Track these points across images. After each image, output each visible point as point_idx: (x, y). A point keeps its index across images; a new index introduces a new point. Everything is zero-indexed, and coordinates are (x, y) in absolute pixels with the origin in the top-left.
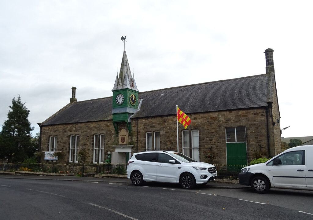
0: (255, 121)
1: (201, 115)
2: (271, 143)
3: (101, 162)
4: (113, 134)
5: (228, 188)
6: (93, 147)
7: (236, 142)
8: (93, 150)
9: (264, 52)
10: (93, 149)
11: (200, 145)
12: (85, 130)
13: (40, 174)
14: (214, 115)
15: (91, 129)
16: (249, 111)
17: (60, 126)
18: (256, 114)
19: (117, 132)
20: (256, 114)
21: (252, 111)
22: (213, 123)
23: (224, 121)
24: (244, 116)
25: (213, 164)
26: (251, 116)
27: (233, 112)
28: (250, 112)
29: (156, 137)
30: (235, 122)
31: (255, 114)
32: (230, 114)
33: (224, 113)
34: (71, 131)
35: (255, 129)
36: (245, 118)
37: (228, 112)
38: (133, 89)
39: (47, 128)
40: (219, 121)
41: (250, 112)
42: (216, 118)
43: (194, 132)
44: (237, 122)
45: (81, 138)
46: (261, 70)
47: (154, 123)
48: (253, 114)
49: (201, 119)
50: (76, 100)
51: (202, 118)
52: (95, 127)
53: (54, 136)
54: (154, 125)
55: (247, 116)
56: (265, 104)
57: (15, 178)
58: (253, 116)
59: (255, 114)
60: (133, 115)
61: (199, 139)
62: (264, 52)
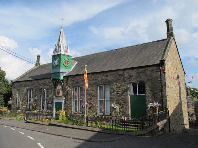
0: (151, 76)
1: (111, 73)
2: (164, 95)
3: (100, 113)
4: (53, 88)
5: (84, 130)
6: (41, 98)
7: (138, 95)
8: (41, 100)
9: (166, 22)
10: (41, 99)
11: (110, 98)
12: (36, 85)
13: (154, 130)
14: (121, 73)
15: (40, 85)
16: (147, 68)
17: (23, 82)
18: (152, 71)
19: (55, 87)
20: (152, 71)
21: (149, 69)
22: (120, 79)
23: (128, 77)
24: (143, 72)
25: (172, 114)
26: (148, 72)
27: (135, 70)
28: (147, 69)
29: (100, 90)
30: (136, 78)
31: (152, 71)
32: (132, 71)
33: (128, 71)
34: (28, 86)
35: (152, 83)
36: (144, 74)
37: (131, 70)
38: (66, 54)
39: (16, 84)
40: (124, 78)
41: (147, 69)
42: (122, 74)
43: (107, 87)
44: (138, 78)
45: (34, 91)
46: (163, 35)
47: (79, 80)
48: (150, 71)
49: (112, 76)
50: (39, 64)
51: (112, 75)
52: (42, 83)
53: (31, 89)
54: (79, 81)
55: (145, 72)
56: (158, 62)
57: (73, 128)
58: (150, 72)
59: (152, 71)
60: (66, 74)
61: (110, 92)
62: (166, 22)
